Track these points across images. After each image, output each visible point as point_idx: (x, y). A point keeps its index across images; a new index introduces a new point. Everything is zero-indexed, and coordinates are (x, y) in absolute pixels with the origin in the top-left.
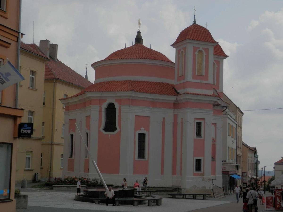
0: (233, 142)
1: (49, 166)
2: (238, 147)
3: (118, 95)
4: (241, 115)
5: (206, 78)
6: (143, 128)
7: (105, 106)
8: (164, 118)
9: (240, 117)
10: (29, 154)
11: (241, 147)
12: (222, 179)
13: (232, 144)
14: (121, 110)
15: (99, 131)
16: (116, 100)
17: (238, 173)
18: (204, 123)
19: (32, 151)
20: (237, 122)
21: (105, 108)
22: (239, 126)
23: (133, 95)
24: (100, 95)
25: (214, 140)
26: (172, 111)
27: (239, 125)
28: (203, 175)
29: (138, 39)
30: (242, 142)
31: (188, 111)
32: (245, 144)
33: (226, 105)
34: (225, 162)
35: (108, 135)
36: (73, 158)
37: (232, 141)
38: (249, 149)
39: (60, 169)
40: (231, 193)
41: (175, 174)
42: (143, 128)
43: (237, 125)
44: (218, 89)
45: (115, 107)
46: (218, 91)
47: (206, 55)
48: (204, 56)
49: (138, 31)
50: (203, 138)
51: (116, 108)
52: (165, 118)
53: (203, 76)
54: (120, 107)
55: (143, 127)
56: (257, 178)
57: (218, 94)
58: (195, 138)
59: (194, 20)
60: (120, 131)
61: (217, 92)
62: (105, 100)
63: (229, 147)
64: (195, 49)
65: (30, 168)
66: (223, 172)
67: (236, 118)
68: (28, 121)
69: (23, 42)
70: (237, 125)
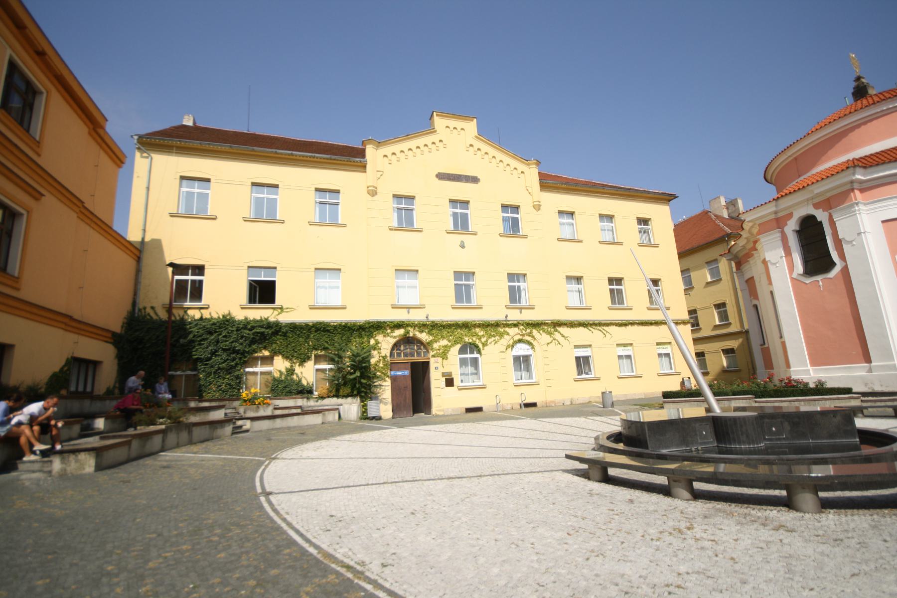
1: (750, 366)
3: (816, 191)
7: (792, 226)
14: (835, 220)
16: (816, 206)
21: (793, 231)
36: (766, 345)
45: (788, 222)
54: (831, 217)
56: (170, 317)
60: (847, 265)
62: (790, 216)
66: (689, 311)
68: (121, 331)
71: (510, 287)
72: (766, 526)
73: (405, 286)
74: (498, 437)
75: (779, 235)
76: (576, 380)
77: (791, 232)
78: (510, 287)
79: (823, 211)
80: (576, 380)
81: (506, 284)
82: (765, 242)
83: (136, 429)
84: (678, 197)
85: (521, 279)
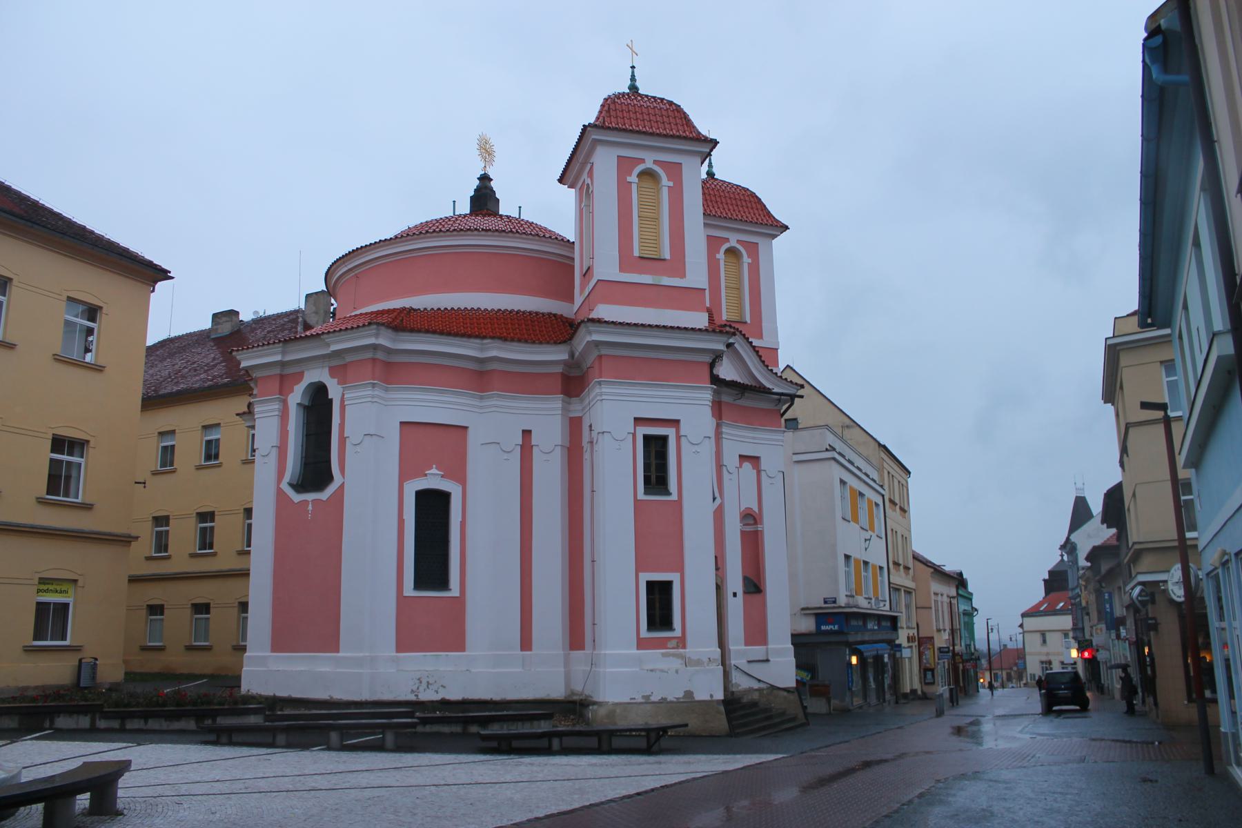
0: (868, 542)
2: (896, 564)
4: (904, 475)
5: (677, 265)
6: (438, 469)
7: (296, 396)
8: (527, 433)
9: (904, 483)
10: (66, 592)
11: (911, 565)
12: (794, 659)
13: (866, 549)
15: (280, 492)
16: (333, 372)
17: (898, 639)
18: (678, 438)
19: (75, 581)
20: (886, 487)
22: (892, 502)
23: (381, 341)
24: (278, 358)
25: (755, 519)
26: (555, 404)
27: (897, 501)
28: (682, 642)
29: (484, 198)
30: (913, 551)
31: (603, 390)
32: (924, 558)
33: (791, 391)
34: (835, 602)
35: (306, 502)
37: (866, 540)
38: (932, 570)
39: (709, 659)
40: (866, 701)
41: (582, 647)
42: (434, 471)
43: (883, 496)
44: (760, 336)
46: (756, 343)
47: (749, 264)
48: (665, 192)
49: (483, 173)
50: (674, 497)
51: (331, 400)
52: (530, 431)
53: (664, 260)
55: (434, 466)
57: (760, 354)
58: (641, 495)
59: (629, 82)
61: (754, 347)
62: (299, 376)
63: (847, 557)
64: (625, 165)
65: (66, 640)
67: (882, 476)
68: (1031, 654)
69: (74, 220)
70: (883, 496)
71: (52, 460)
72: (1126, 610)
73: (203, 530)
74: (119, 751)
75: (276, 406)
76: (29, 650)
77: (295, 405)
78: (52, 460)
79: (338, 384)
80: (29, 650)
81: (45, 455)
82: (262, 412)
83: (146, 723)
84: (172, 278)
85: (77, 450)
